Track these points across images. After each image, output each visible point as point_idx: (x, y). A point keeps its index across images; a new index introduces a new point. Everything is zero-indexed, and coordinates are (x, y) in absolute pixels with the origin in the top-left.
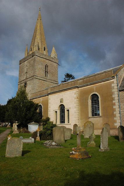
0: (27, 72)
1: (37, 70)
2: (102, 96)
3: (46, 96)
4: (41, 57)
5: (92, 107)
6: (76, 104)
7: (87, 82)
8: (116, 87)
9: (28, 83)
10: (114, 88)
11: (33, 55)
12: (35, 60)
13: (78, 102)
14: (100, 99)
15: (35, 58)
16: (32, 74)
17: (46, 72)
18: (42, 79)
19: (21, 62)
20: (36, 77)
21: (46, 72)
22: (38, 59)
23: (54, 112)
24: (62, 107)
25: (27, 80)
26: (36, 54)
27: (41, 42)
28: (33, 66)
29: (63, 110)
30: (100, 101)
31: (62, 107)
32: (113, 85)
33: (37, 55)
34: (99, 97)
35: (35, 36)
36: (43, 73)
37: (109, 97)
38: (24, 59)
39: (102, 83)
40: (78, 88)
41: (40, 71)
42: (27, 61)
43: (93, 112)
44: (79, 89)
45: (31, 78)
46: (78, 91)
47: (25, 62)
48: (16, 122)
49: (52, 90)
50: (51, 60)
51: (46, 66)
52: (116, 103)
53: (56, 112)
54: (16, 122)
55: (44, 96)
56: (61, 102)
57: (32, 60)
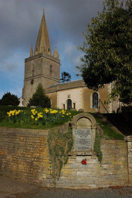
0: (34, 71)
3: (54, 92)
4: (47, 58)
5: (93, 101)
6: (81, 96)
8: (110, 88)
9: (35, 80)
10: (109, 89)
11: (40, 55)
12: (42, 61)
13: (82, 101)
14: (99, 96)
15: (42, 58)
16: (39, 73)
17: (50, 71)
18: (47, 77)
19: (26, 60)
20: (43, 76)
21: (51, 71)
22: (44, 59)
23: (62, 105)
24: (69, 102)
25: (34, 77)
26: (43, 55)
27: (46, 43)
28: (40, 66)
29: (70, 103)
31: (69, 102)
33: (44, 56)
35: (41, 38)
36: (48, 72)
40: (83, 87)
41: (46, 72)
42: (33, 61)
44: (84, 88)
45: (38, 76)
46: (82, 89)
49: (60, 87)
50: (55, 60)
51: (51, 66)
53: (64, 105)
55: (53, 92)
56: (68, 97)
57: (39, 60)
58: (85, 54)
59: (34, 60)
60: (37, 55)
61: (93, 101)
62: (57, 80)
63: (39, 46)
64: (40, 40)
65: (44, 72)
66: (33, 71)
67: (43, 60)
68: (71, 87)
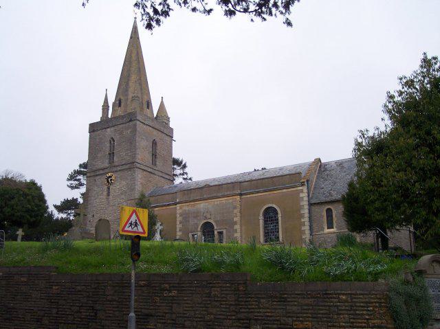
0: (113, 153)
1: (138, 151)
2: (284, 212)
7: (257, 188)
8: (306, 199)
14: (280, 215)
15: (135, 125)
17: (153, 155)
18: (146, 168)
20: (138, 165)
21: (154, 155)
22: (140, 126)
28: (131, 142)
30: (280, 218)
32: (301, 195)
34: (279, 212)
35: (129, 76)
36: (149, 157)
37: (295, 213)
38: (156, 149)
39: (284, 190)
42: (112, 129)
43: (266, 234)
47: (109, 130)
48: (20, 232)
51: (154, 143)
52: (306, 223)
54: (20, 232)
55: (165, 206)
58: (400, 88)
59: (116, 128)
60: (123, 117)
61: (265, 228)
62: (167, 177)
63: (127, 95)
64: (128, 80)
65: (139, 158)
66: (112, 154)
67: (138, 129)
68: (161, 208)
